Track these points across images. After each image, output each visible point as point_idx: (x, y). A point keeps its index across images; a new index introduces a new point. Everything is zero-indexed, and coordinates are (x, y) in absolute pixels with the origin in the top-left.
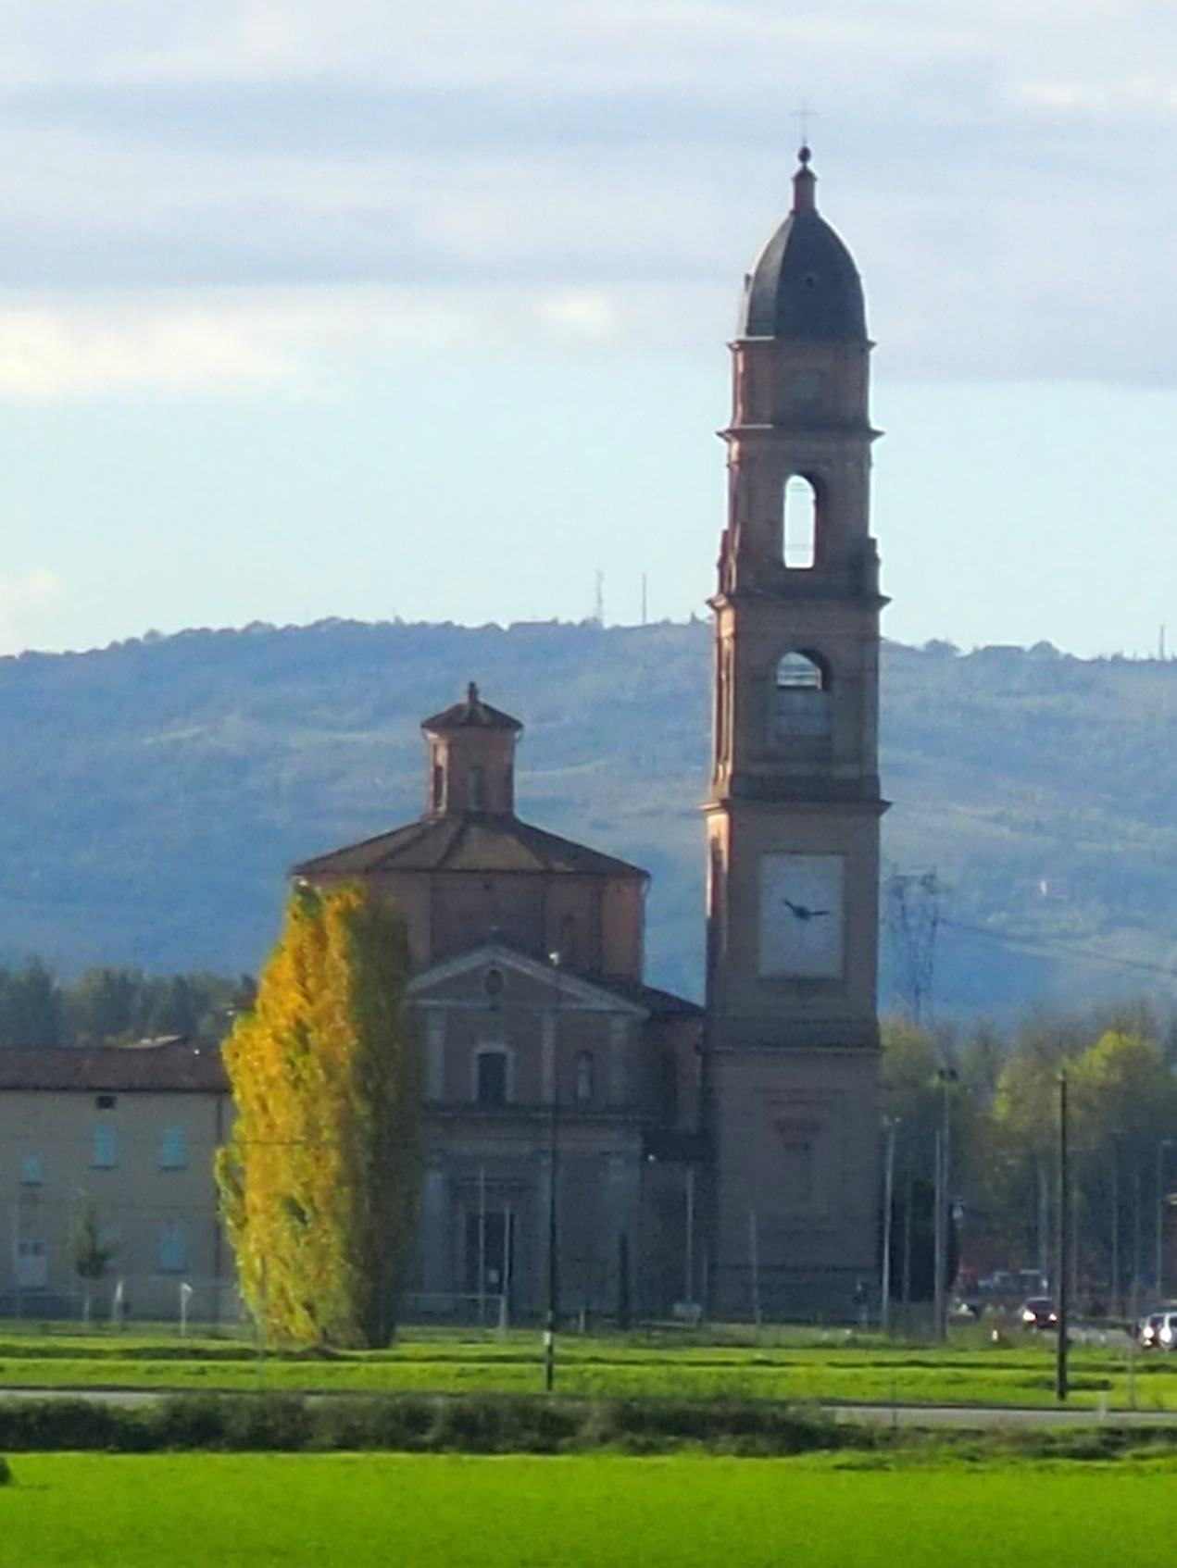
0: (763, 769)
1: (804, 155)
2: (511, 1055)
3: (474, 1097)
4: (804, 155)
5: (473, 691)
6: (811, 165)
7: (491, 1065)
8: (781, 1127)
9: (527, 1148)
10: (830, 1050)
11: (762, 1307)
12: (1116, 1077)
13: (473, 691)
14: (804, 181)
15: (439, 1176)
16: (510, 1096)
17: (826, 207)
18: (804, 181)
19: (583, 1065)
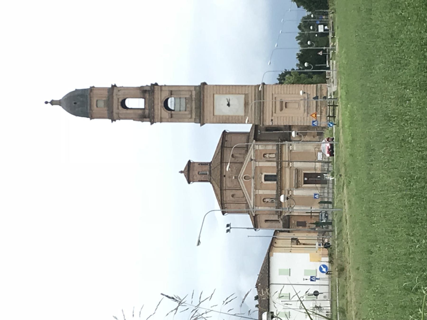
0: (194, 116)
1: (46, 103)
2: (265, 173)
3: (275, 182)
4: (46, 103)
5: (181, 172)
6: (49, 101)
7: (267, 178)
8: (281, 109)
9: (288, 170)
10: (240, 182)
11: (410, 255)
12: (300, 52)
13: (181, 172)
14: (53, 103)
15: (294, 191)
16: (275, 174)
17: (59, 97)
18: (53, 103)
19: (267, 156)
